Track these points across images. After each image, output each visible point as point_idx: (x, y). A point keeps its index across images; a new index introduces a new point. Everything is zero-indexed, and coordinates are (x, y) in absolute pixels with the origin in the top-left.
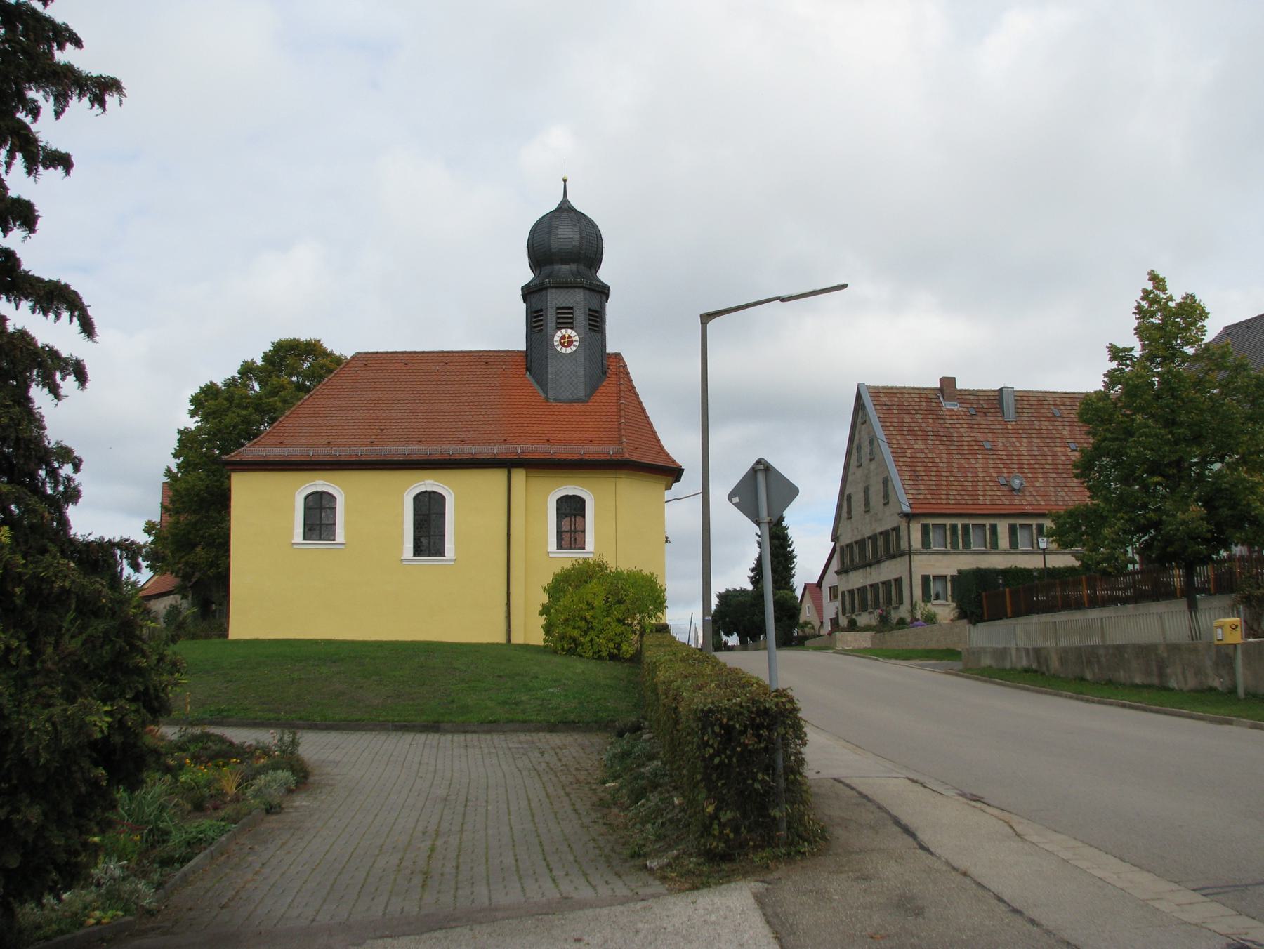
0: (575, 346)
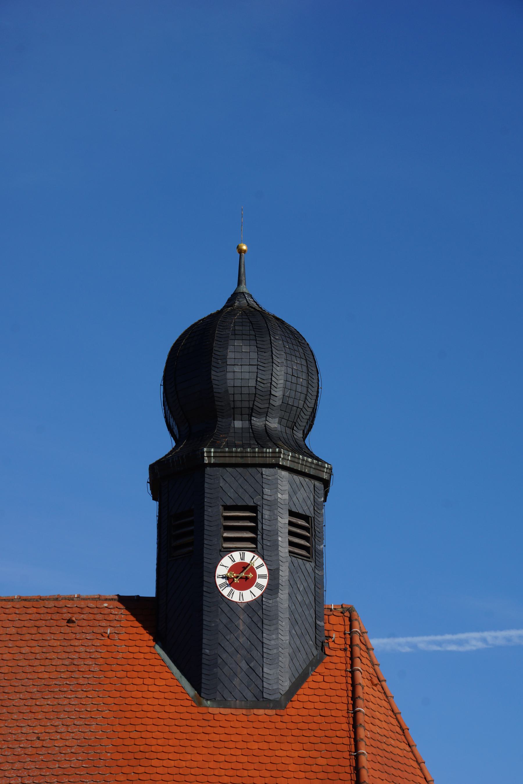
0: (259, 586)
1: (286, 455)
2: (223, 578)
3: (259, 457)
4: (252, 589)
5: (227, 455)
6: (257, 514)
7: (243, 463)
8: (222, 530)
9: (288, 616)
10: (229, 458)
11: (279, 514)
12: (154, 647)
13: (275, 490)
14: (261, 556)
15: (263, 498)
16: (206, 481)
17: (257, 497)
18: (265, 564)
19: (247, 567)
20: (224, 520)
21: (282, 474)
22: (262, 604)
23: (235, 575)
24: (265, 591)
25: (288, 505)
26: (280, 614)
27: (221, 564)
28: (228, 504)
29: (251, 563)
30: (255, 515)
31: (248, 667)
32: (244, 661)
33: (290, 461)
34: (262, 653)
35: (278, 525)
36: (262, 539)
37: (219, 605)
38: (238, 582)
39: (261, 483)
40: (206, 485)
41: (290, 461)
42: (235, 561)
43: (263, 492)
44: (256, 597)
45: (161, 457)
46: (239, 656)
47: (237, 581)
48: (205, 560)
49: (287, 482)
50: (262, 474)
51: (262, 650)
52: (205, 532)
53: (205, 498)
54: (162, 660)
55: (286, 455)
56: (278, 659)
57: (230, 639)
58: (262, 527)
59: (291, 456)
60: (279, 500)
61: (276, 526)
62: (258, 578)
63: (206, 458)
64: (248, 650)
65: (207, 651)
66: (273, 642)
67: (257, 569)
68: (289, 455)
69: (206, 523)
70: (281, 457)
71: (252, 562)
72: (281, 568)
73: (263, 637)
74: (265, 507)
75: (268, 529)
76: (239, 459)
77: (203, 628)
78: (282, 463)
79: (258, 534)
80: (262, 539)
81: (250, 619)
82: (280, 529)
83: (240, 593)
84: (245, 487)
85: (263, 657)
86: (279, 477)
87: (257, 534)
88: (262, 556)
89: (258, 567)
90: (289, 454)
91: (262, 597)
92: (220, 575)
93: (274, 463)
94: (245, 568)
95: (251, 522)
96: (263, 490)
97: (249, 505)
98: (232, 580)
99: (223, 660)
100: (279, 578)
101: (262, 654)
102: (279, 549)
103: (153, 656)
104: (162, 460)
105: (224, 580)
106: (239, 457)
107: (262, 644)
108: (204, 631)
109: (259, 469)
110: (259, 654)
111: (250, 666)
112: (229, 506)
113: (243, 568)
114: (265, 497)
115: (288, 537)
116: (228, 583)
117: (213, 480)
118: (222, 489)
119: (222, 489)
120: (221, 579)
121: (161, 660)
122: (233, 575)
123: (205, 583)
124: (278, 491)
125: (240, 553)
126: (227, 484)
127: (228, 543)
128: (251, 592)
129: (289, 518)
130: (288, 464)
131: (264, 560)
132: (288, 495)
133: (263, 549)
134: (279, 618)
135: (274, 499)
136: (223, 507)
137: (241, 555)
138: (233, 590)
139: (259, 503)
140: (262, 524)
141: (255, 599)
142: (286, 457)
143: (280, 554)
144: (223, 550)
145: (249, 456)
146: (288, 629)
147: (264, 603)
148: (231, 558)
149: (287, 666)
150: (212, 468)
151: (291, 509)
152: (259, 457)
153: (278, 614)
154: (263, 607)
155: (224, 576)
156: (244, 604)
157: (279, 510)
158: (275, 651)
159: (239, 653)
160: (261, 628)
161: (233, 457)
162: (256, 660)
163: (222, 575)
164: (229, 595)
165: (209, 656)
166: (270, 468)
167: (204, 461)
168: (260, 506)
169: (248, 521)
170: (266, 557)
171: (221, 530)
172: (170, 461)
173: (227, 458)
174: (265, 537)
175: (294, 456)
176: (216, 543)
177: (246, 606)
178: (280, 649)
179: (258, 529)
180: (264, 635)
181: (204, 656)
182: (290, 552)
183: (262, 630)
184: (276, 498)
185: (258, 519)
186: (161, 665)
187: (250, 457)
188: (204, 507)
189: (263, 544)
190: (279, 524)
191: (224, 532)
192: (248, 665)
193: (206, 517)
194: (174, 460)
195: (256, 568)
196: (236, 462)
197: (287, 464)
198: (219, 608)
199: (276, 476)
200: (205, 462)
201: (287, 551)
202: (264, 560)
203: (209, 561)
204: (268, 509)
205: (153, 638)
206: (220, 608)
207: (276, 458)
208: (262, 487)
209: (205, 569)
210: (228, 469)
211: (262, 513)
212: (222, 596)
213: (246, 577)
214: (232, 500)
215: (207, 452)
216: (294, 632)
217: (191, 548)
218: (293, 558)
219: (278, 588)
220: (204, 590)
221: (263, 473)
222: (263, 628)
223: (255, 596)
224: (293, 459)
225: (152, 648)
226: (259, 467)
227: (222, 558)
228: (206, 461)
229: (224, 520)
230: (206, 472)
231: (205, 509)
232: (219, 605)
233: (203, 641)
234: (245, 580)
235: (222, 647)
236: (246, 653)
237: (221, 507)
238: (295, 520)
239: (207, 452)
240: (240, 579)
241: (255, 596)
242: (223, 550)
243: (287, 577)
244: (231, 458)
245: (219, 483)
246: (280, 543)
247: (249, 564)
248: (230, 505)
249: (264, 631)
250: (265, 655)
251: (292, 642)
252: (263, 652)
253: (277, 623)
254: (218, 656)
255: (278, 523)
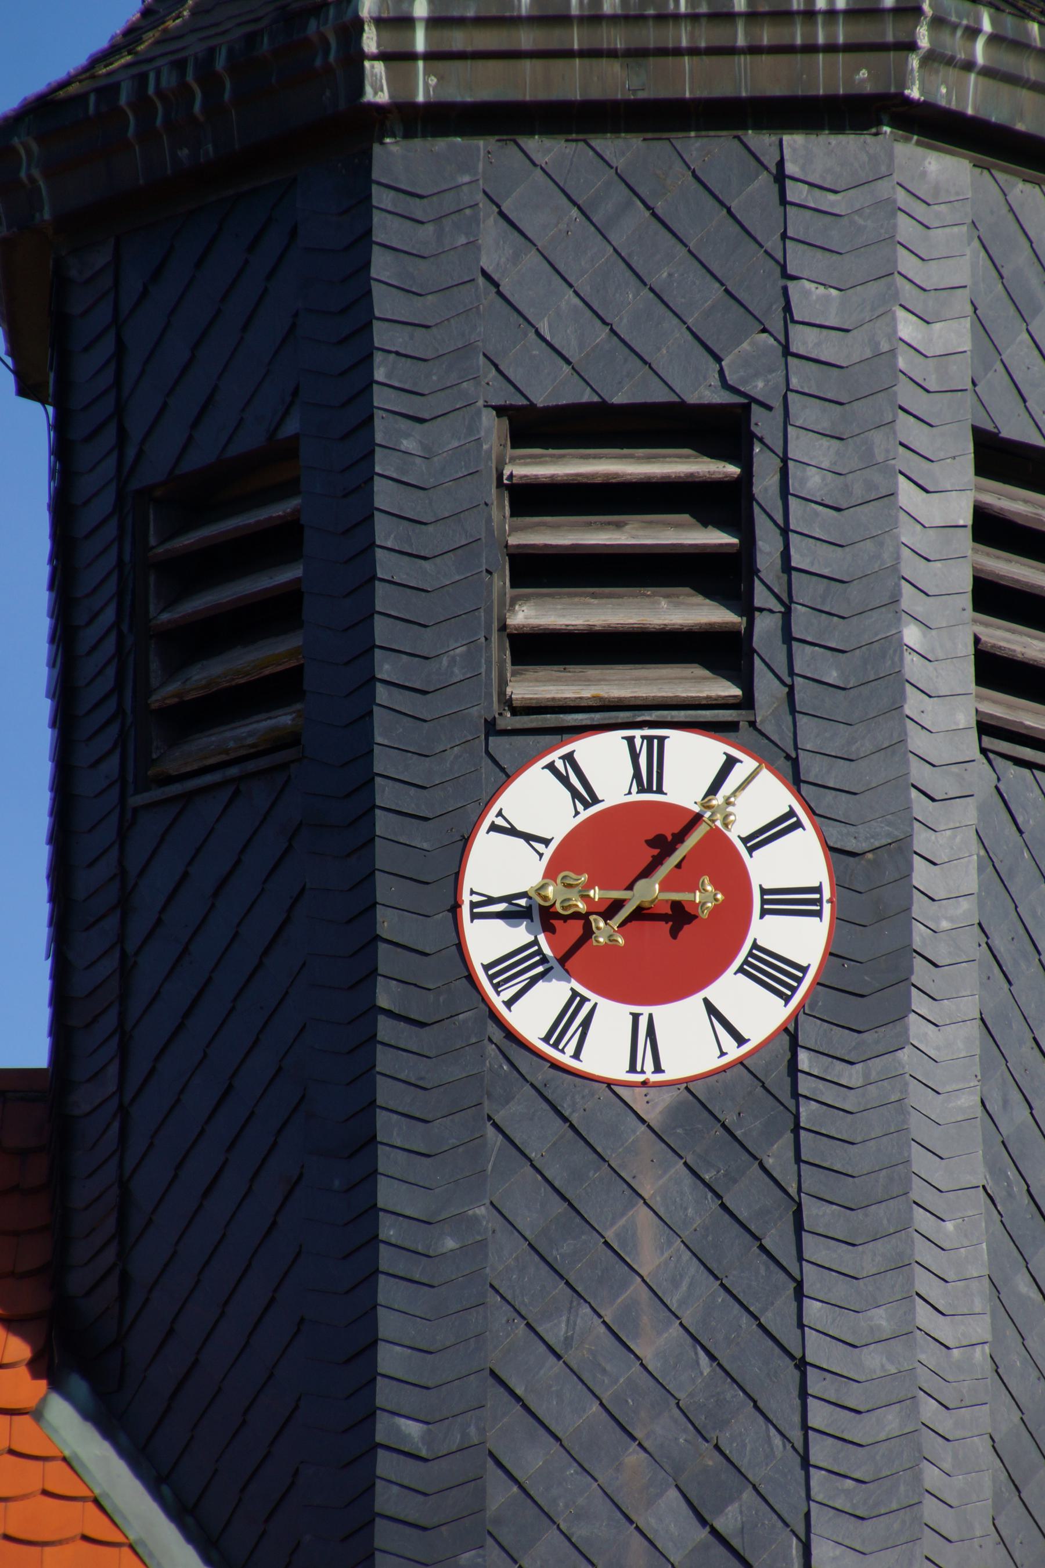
1: (955, 27)
2: (508, 916)
3: (754, 50)
4: (714, 992)
5: (526, 39)
6: (747, 464)
7: (641, 95)
8: (501, 581)
9: (980, 1176)
10: (538, 63)
11: (904, 460)
12: (37, 1414)
13: (874, 288)
14: (782, 762)
15: (786, 351)
16: (378, 235)
17: (745, 346)
18: (812, 812)
19: (680, 837)
20: (517, 511)
21: (924, 174)
22: (795, 1095)
23: (595, 893)
24: (812, 1006)
25: (969, 398)
26: (920, 1161)
27: (500, 822)
28: (541, 400)
29: (707, 806)
30: (733, 470)
31: (704, 1533)
32: (673, 1494)
33: (987, 72)
34: (796, 1435)
35: (897, 537)
36: (788, 637)
37: (487, 1107)
38: (621, 941)
39: (772, 242)
40: (381, 266)
41: (987, 72)
42: (596, 800)
43: (788, 308)
44: (746, 1048)
45: (58, 74)
46: (634, 1457)
47: (610, 938)
48: (385, 794)
49: (964, 228)
50: (780, 177)
51: (797, 1419)
52: (383, 598)
53: (378, 357)
54: (96, 1502)
55: (955, 27)
56: (918, 1479)
57: (568, 1341)
58: (786, 555)
59: (994, 39)
60: (901, 363)
61: (881, 544)
62: (764, 913)
63: (379, 67)
64: (700, 1420)
65: (413, 1429)
66: (873, 1360)
67: (751, 850)
68: (973, 32)
69: (385, 533)
70: (912, 46)
71: (718, 800)
72: (922, 840)
73: (801, 1326)
74: (803, 412)
75: (826, 572)
76: (614, 68)
77: (377, 1272)
78: (922, 91)
79: (757, 603)
80: (788, 637)
81: (713, 1204)
82: (910, 566)
83: (636, 1017)
84: (660, 277)
85: (806, 1464)
86: (901, 196)
87: (748, 610)
88: (788, 757)
89: (757, 840)
90: (978, 19)
91: (794, 1045)
92: (496, 894)
93: (868, 89)
94: (664, 846)
95: (705, 521)
96: (785, 290)
97: (692, 398)
98: (576, 928)
99: (521, 1487)
100: (908, 909)
101: (799, 1445)
102: (907, 711)
103: (32, 1475)
104: (61, 93)
105: (519, 935)
106: (612, 54)
107: (797, 1374)
108: (387, 1291)
109: (761, 141)
110: (777, 1440)
111: (714, 1532)
112: (547, 409)
113: (651, 843)
114: (803, 340)
115: (975, 621)
116: (547, 950)
117: (430, 228)
118: (499, 293)
119: (499, 293)
120: (499, 923)
121: (91, 1507)
122: (585, 898)
123: (386, 959)
124: (893, 296)
125: (630, 740)
126: (532, 258)
127: (544, 672)
128: (711, 1009)
129: (979, 489)
131: (804, 787)
132: (967, 323)
133: (793, 711)
134: (919, 1191)
135: (868, 353)
136: (505, 421)
137: (635, 756)
138: (584, 1000)
139: (760, 384)
140: (785, 531)
141: (740, 1062)
142: (955, 44)
143: (917, 741)
144: (508, 721)
145: (684, 43)
146: (978, 1268)
147: (805, 1086)
148: (564, 780)
149: (982, 1527)
150: (418, 143)
151: (990, 427)
152: (754, 50)
153: (908, 1162)
154: (797, 1117)
155: (523, 902)
156: (667, 1097)
157: (908, 429)
158: (891, 1421)
159: (633, 1438)
160: (789, 1261)
161: (568, 54)
162: (755, 1487)
163: (507, 899)
164: (555, 1035)
165: (425, 1460)
166: (838, 128)
167: (360, 91)
168: (769, 408)
169: (686, 517)
170: (812, 768)
171: (497, 583)
172: (123, 100)
173: (527, 64)
174: (802, 623)
175: (1010, 34)
176: (458, 674)
177: (675, 1113)
178: (929, 1409)
179: (754, 571)
180: (813, 1309)
181: (386, 1464)
182: (986, 728)
183: (796, 1274)
184: (885, 347)
185: (751, 498)
186: (85, 1538)
187: (694, 51)
188: (371, 418)
189: (792, 673)
190: (909, 534)
191: (514, 601)
192: (703, 1522)
193: (384, 495)
194: (151, 90)
195: (745, 840)
196: (596, 93)
197: (962, 97)
198: (490, 1131)
199: (883, 189)
200: (370, 95)
201: (965, 718)
202: (804, 787)
203: (409, 800)
204: (824, 426)
205: (32, 1351)
206: (495, 1125)
207: (882, 55)
208: (784, 267)
209: (383, 856)
210: (533, 144)
211: (785, 460)
212: (513, 1051)
213: (677, 905)
214: (566, 369)
215: (379, 22)
216: (1024, 1287)
217: (284, 719)
218: (1013, 771)
219: (903, 981)
220: (383, 1001)
221: (790, 168)
222: (800, 1258)
223: (741, 1040)
224: (1008, 61)
225: (24, 1422)
226: (759, 126)
227: (508, 777)
228: (378, 89)
229: (514, 514)
230: (375, 175)
231: (379, 438)
232: (487, 1107)
233: (379, 1427)
234: (665, 927)
235: (518, 1399)
236: (684, 1436)
237: (489, 420)
238: (1026, 501)
239: (379, 22)
240: (634, 924)
241: (741, 1040)
242: (508, 721)
243: (965, 905)
244: (559, 65)
245: (472, 245)
246: (913, 667)
247: (697, 818)
248: (553, 402)
249: (811, 1276)
250: (820, 1452)
251: (1015, 1360)
252: (805, 1428)
253: (905, 1226)
254: (490, 1463)
255: (896, 525)
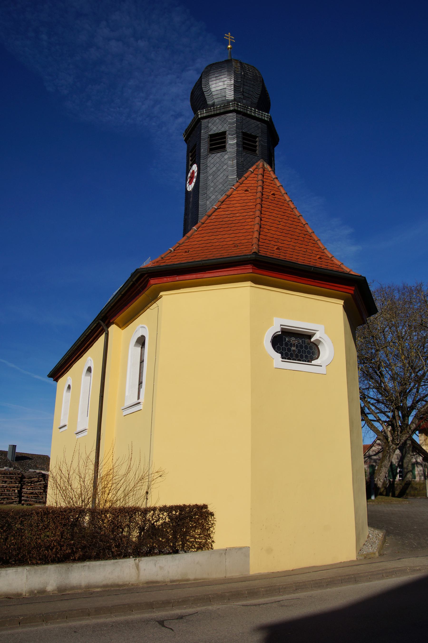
130: (205, 115)
